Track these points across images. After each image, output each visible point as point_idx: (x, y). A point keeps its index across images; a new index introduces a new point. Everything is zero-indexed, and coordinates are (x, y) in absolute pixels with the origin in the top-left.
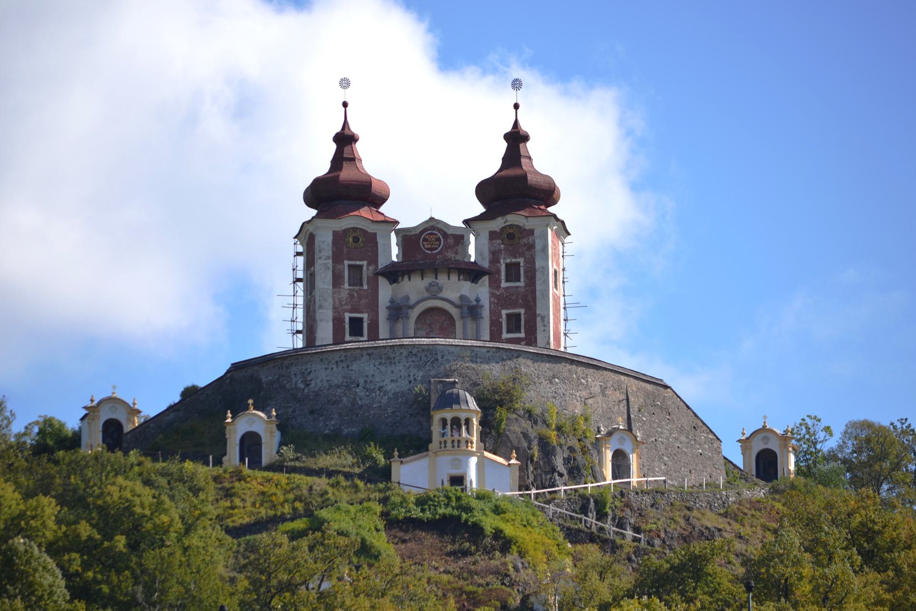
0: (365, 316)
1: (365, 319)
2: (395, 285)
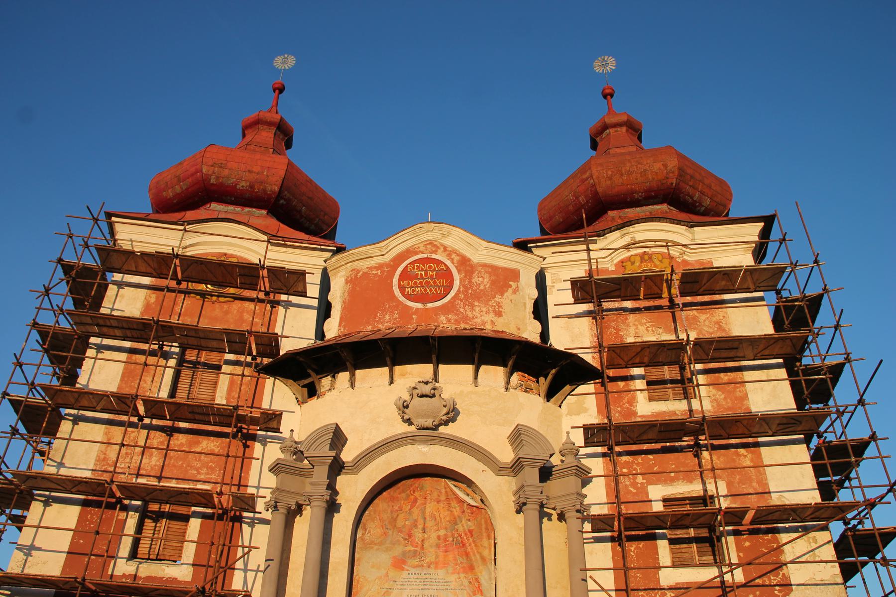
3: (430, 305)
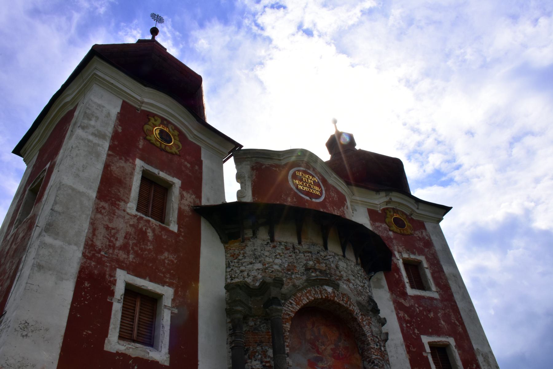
1: (167, 301)
2: (235, 246)
3: (314, 200)
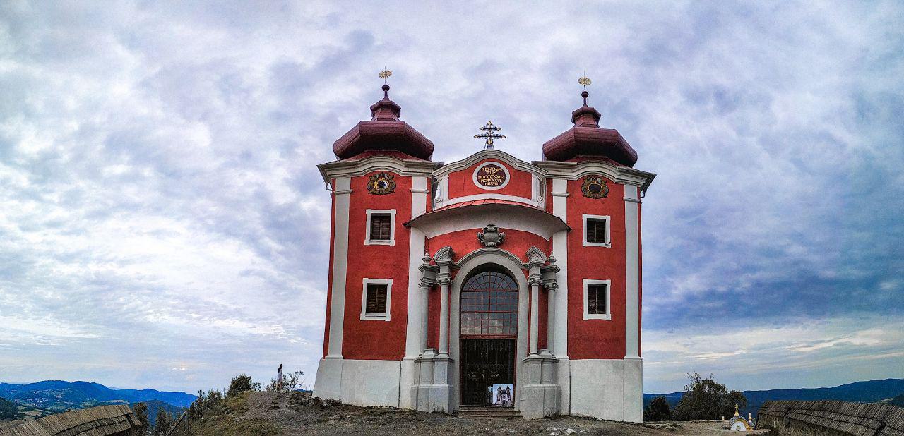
0: (389, 282)
